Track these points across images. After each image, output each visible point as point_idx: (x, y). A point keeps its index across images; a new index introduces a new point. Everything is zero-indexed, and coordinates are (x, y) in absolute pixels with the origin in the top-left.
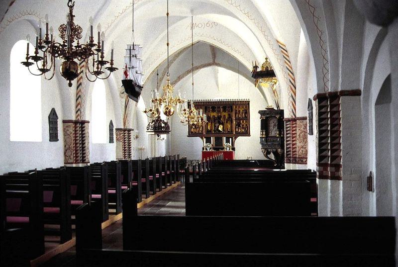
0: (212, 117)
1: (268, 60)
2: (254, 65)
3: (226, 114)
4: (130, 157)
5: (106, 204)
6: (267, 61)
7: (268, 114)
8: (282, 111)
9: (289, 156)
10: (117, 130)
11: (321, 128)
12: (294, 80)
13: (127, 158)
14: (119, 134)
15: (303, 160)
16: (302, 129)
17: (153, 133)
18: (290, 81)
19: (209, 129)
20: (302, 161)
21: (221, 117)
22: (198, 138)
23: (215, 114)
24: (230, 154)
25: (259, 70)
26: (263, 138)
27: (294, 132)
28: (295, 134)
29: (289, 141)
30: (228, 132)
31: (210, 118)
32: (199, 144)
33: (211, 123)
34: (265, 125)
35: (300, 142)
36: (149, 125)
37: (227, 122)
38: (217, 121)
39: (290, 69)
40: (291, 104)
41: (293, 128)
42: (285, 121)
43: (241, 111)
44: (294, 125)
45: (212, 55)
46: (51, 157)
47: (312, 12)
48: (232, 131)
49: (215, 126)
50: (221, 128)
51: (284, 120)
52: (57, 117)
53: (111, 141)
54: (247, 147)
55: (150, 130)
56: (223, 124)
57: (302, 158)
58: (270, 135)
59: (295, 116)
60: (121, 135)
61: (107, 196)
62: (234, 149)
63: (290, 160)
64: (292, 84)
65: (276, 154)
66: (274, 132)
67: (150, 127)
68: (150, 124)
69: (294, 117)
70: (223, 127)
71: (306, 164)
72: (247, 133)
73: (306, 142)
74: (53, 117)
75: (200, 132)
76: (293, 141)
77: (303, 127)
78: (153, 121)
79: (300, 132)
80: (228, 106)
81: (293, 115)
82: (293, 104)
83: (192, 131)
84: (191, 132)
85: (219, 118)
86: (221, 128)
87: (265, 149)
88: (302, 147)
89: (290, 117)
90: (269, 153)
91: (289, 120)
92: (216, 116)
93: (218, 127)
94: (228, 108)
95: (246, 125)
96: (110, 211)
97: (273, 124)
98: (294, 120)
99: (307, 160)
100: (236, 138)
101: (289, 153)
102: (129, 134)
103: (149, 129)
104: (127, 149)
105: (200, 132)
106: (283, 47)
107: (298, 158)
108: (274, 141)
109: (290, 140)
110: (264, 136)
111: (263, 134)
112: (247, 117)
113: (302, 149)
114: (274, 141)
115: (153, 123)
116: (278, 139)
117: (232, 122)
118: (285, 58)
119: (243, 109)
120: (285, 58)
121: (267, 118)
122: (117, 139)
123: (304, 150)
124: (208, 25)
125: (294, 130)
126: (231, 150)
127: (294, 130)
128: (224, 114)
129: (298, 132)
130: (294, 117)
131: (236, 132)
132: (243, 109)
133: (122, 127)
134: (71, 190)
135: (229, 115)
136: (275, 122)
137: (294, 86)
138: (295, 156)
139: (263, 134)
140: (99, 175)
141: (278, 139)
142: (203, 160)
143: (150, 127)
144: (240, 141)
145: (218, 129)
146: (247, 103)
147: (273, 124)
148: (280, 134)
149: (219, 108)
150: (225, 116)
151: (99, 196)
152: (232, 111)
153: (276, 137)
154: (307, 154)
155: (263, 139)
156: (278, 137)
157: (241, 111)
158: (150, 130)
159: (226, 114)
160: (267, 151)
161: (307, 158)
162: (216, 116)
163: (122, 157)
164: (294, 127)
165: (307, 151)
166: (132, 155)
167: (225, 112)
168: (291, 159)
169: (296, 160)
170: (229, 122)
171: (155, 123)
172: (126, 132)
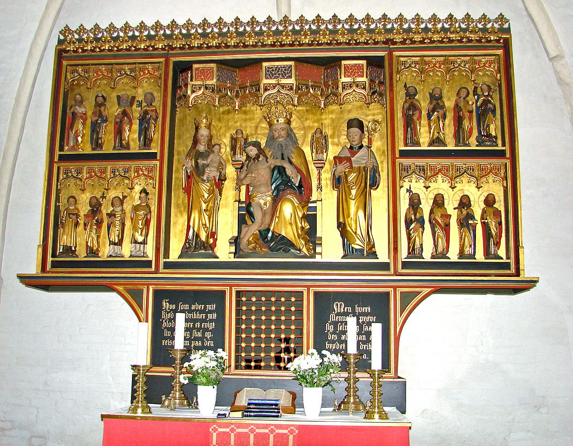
22: (113, 303)
38: (262, 172)
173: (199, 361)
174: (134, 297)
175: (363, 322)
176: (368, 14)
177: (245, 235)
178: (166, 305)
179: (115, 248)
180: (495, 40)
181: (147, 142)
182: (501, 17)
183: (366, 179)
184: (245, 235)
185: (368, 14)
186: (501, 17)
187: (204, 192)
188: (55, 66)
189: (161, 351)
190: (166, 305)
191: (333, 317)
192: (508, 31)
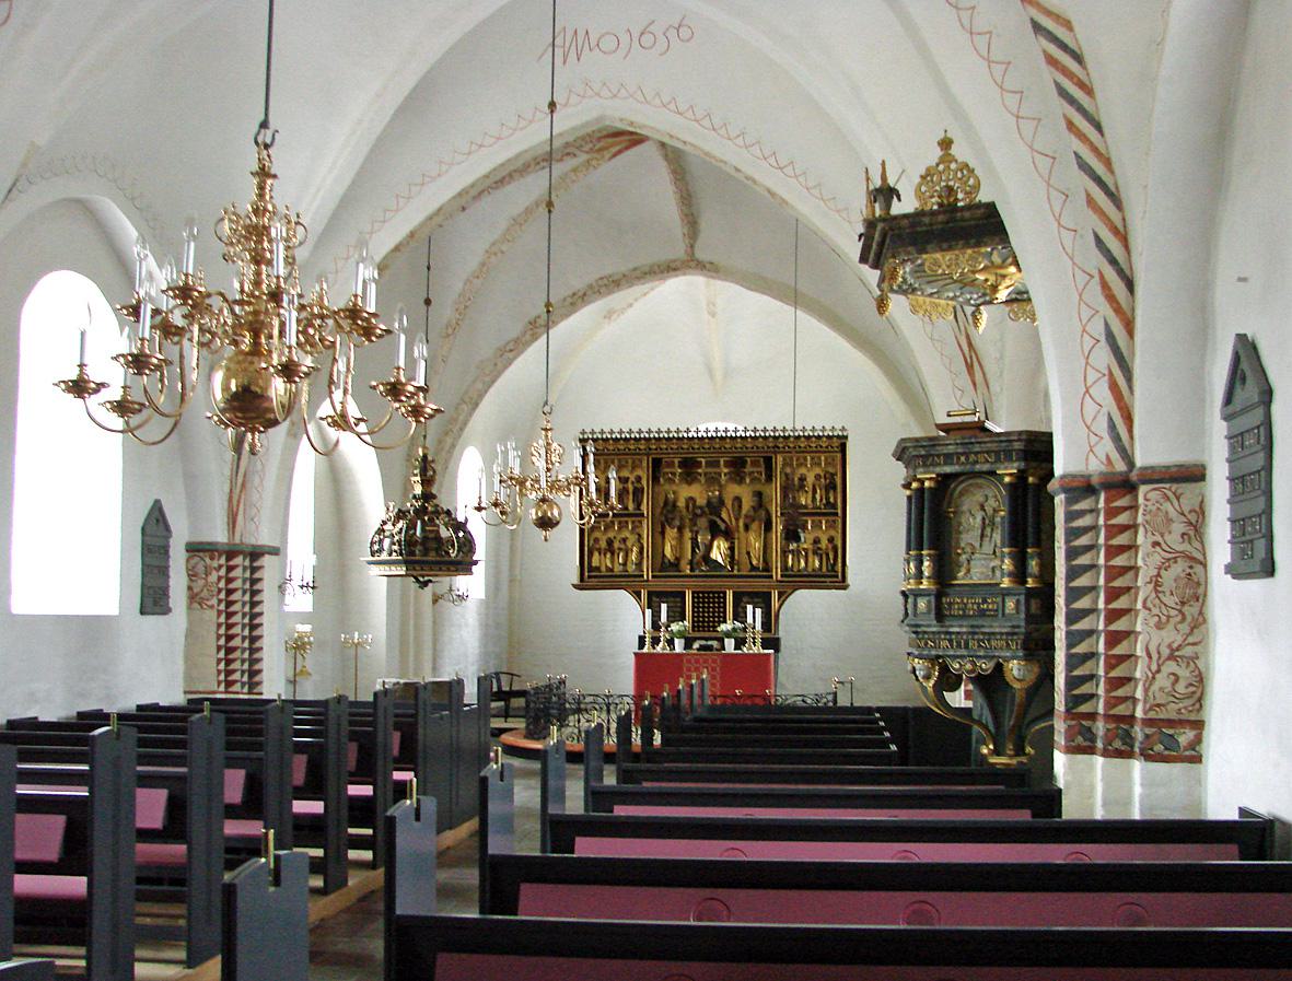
0: (681, 503)
1: (954, 150)
2: (878, 183)
3: (745, 493)
4: (253, 685)
5: (341, 831)
6: (947, 158)
7: (948, 459)
8: (1037, 448)
9: (1084, 708)
10: (194, 549)
11: (1070, 582)
12: (1124, 239)
13: (237, 687)
14: (201, 568)
15: (1175, 736)
16: (1174, 540)
17: (402, 570)
18: (1099, 241)
19: (668, 552)
20: (1171, 743)
21: (721, 502)
22: (623, 599)
23: (697, 492)
24: (760, 669)
25: (904, 206)
26: (917, 594)
27: (1119, 561)
28: (1124, 570)
29: (1085, 613)
30: (754, 568)
31: (674, 505)
32: (623, 619)
33: (680, 530)
34: (932, 523)
35: (1159, 626)
36: (381, 531)
37: (747, 528)
38: (703, 522)
39: (1100, 169)
40: (1102, 392)
41: (1113, 530)
42: (1066, 490)
43: (810, 479)
44: (1122, 519)
45: (674, 205)
46: (157, 669)
47: (1057, 215)
48: (767, 568)
49: (695, 544)
50: (719, 552)
51: (1052, 486)
52: (167, 528)
53: (153, 600)
54: (846, 634)
55: (384, 556)
56: (728, 535)
57: (1170, 723)
58: (961, 578)
59: (1131, 464)
60: (213, 577)
61: (390, 787)
62: (772, 643)
63: (1090, 735)
64: (1113, 261)
65: (991, 685)
66: (985, 560)
67: (387, 542)
68: (389, 527)
69: (1120, 466)
70: (731, 549)
71: (1197, 759)
72: (832, 575)
73: (1199, 622)
74: (154, 533)
75: (631, 568)
76: (1113, 616)
77: (1178, 527)
78: (401, 515)
79: (1157, 559)
80: (751, 457)
81: (1115, 456)
82: (1114, 386)
83: (595, 562)
84: (591, 569)
85: (714, 507)
86: (719, 552)
87: (934, 660)
88: (1171, 657)
89: (1095, 467)
90: (949, 681)
91: (1082, 488)
92: (701, 501)
93: (709, 548)
94: (755, 464)
95: (831, 540)
96: (353, 854)
97: (980, 519)
98: (1123, 485)
99: (1198, 740)
100: (783, 596)
101: (1085, 689)
102: (254, 570)
103: (380, 551)
104: (238, 637)
105: (631, 568)
106: (1060, 32)
107: (1149, 722)
108: (982, 614)
109: (1093, 611)
110: (925, 585)
111: (919, 575)
112: (834, 506)
113: (1171, 667)
114: (982, 614)
115: (401, 524)
116: (1010, 604)
117: (768, 527)
118: (1072, 101)
119: (818, 470)
120: (1072, 101)
121: (944, 481)
122: (194, 597)
123: (1184, 673)
124: (647, 40)
125: (1122, 549)
126: (757, 649)
127: (1122, 549)
128: (733, 490)
129: (1146, 561)
130: (1120, 466)
131: (785, 568)
132: (818, 470)
133: (220, 536)
134: (222, 779)
135: (759, 495)
136: (992, 503)
137: (1120, 272)
138: (1121, 710)
139: (919, 575)
140: (369, 716)
141: (1010, 604)
142: (638, 697)
143: (387, 542)
144: (805, 611)
145: (707, 558)
146: (836, 443)
147: (980, 519)
148: (1020, 575)
149: (716, 464)
150: (738, 500)
151: (367, 790)
152: (769, 478)
153: (991, 589)
154: (1199, 701)
155: (922, 604)
156: (1006, 593)
157: (810, 479)
158: (384, 556)
159: (745, 493)
160: (945, 669)
161: (1199, 725)
162: (701, 501)
163: (211, 684)
164: (1123, 528)
165: (1200, 681)
166: (265, 676)
167: (741, 481)
168: (1100, 727)
169: (1128, 738)
170: (754, 526)
171: (411, 526)
172: (238, 560)
173: (675, 627)
174: (637, 595)
175: (900, 287)
176: (1240, 808)
177: (1125, 227)
178: (654, 599)
179: (435, 669)
180: (836, 447)
181: (638, 506)
182: (843, 429)
183: (739, 548)
184: (1125, 227)
185: (1240, 808)
186: (843, 429)
187: (730, 507)
188: (1174, 470)
189: (656, 626)
190: (654, 599)
191: (743, 604)
192: (846, 437)
